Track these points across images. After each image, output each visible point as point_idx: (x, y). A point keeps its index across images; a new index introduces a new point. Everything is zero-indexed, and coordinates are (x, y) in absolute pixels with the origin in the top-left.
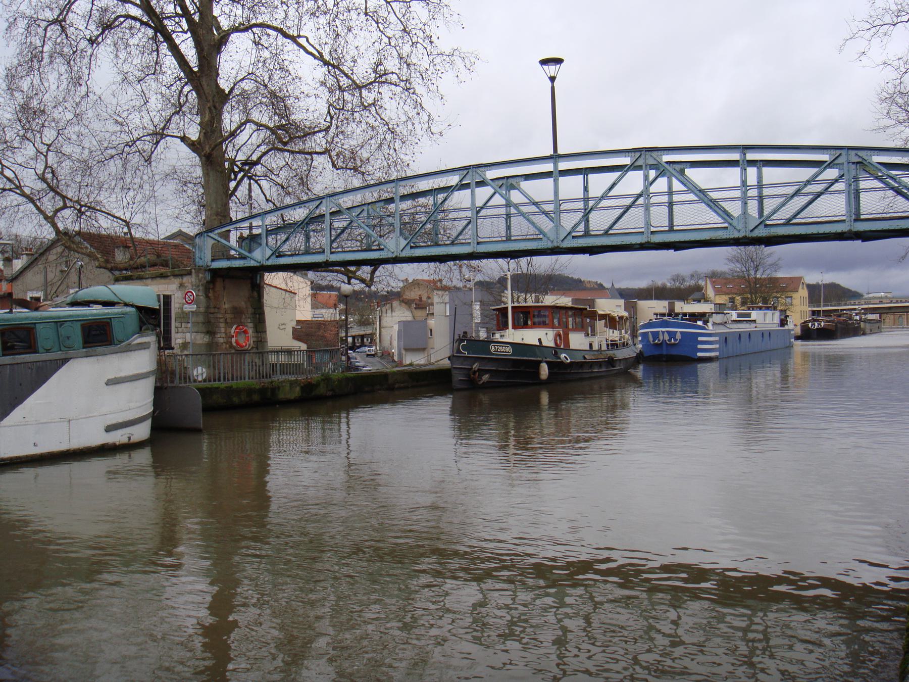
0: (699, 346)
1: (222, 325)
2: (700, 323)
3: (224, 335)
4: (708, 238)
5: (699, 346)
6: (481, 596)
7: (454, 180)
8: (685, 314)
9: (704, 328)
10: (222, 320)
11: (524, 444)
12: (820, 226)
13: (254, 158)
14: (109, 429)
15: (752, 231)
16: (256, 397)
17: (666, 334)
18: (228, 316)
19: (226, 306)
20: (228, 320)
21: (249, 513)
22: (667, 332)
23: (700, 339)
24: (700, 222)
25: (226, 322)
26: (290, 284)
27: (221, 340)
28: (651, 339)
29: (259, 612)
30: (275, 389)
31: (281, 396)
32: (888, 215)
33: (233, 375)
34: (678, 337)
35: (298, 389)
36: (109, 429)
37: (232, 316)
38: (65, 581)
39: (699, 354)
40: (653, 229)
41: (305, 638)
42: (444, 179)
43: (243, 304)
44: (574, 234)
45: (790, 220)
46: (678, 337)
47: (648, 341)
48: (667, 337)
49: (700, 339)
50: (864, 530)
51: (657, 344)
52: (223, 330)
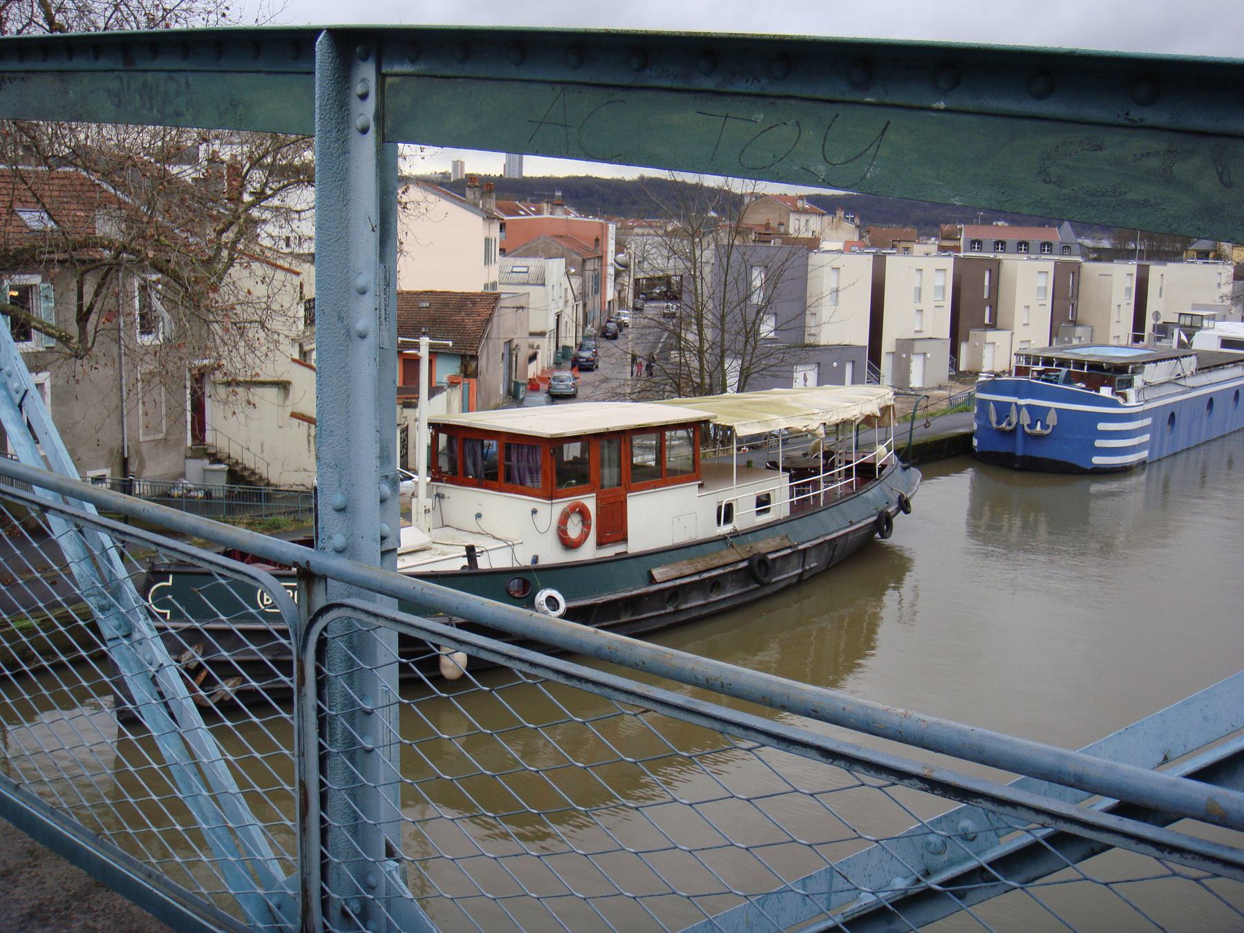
0: (1099, 443)
2: (1105, 392)
5: (1099, 443)
6: (465, 562)
8: (1080, 364)
9: (1114, 404)
11: (1107, 548)
17: (1024, 411)
21: (164, 412)
22: (1028, 407)
23: (1102, 426)
28: (993, 418)
29: (238, 307)
34: (1052, 420)
39: (1098, 460)
41: (257, 375)
46: (1052, 420)
47: (988, 421)
48: (1025, 419)
49: (1102, 426)
51: (1003, 432)
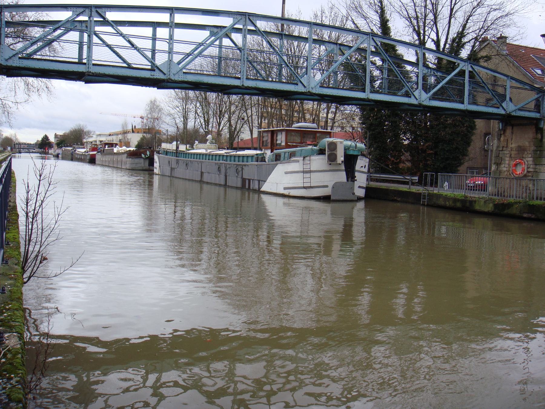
1: (507, 159)
3: (507, 166)
4: (229, 84)
7: (63, 16)
10: (508, 155)
12: (54, 63)
13: (512, 12)
14: (285, 189)
15: (7, 60)
16: (459, 205)
18: (513, 153)
19: (513, 145)
20: (512, 156)
24: (99, 59)
25: (510, 157)
26: (183, 93)
27: (505, 169)
30: (472, 202)
31: (477, 207)
32: (48, 58)
33: (516, 194)
35: (491, 205)
36: (285, 189)
37: (516, 152)
38: (507, 310)
40: (94, 62)
42: (44, 13)
43: (527, 144)
44: (184, 71)
45: (31, 55)
50: (129, 252)
52: (507, 162)
